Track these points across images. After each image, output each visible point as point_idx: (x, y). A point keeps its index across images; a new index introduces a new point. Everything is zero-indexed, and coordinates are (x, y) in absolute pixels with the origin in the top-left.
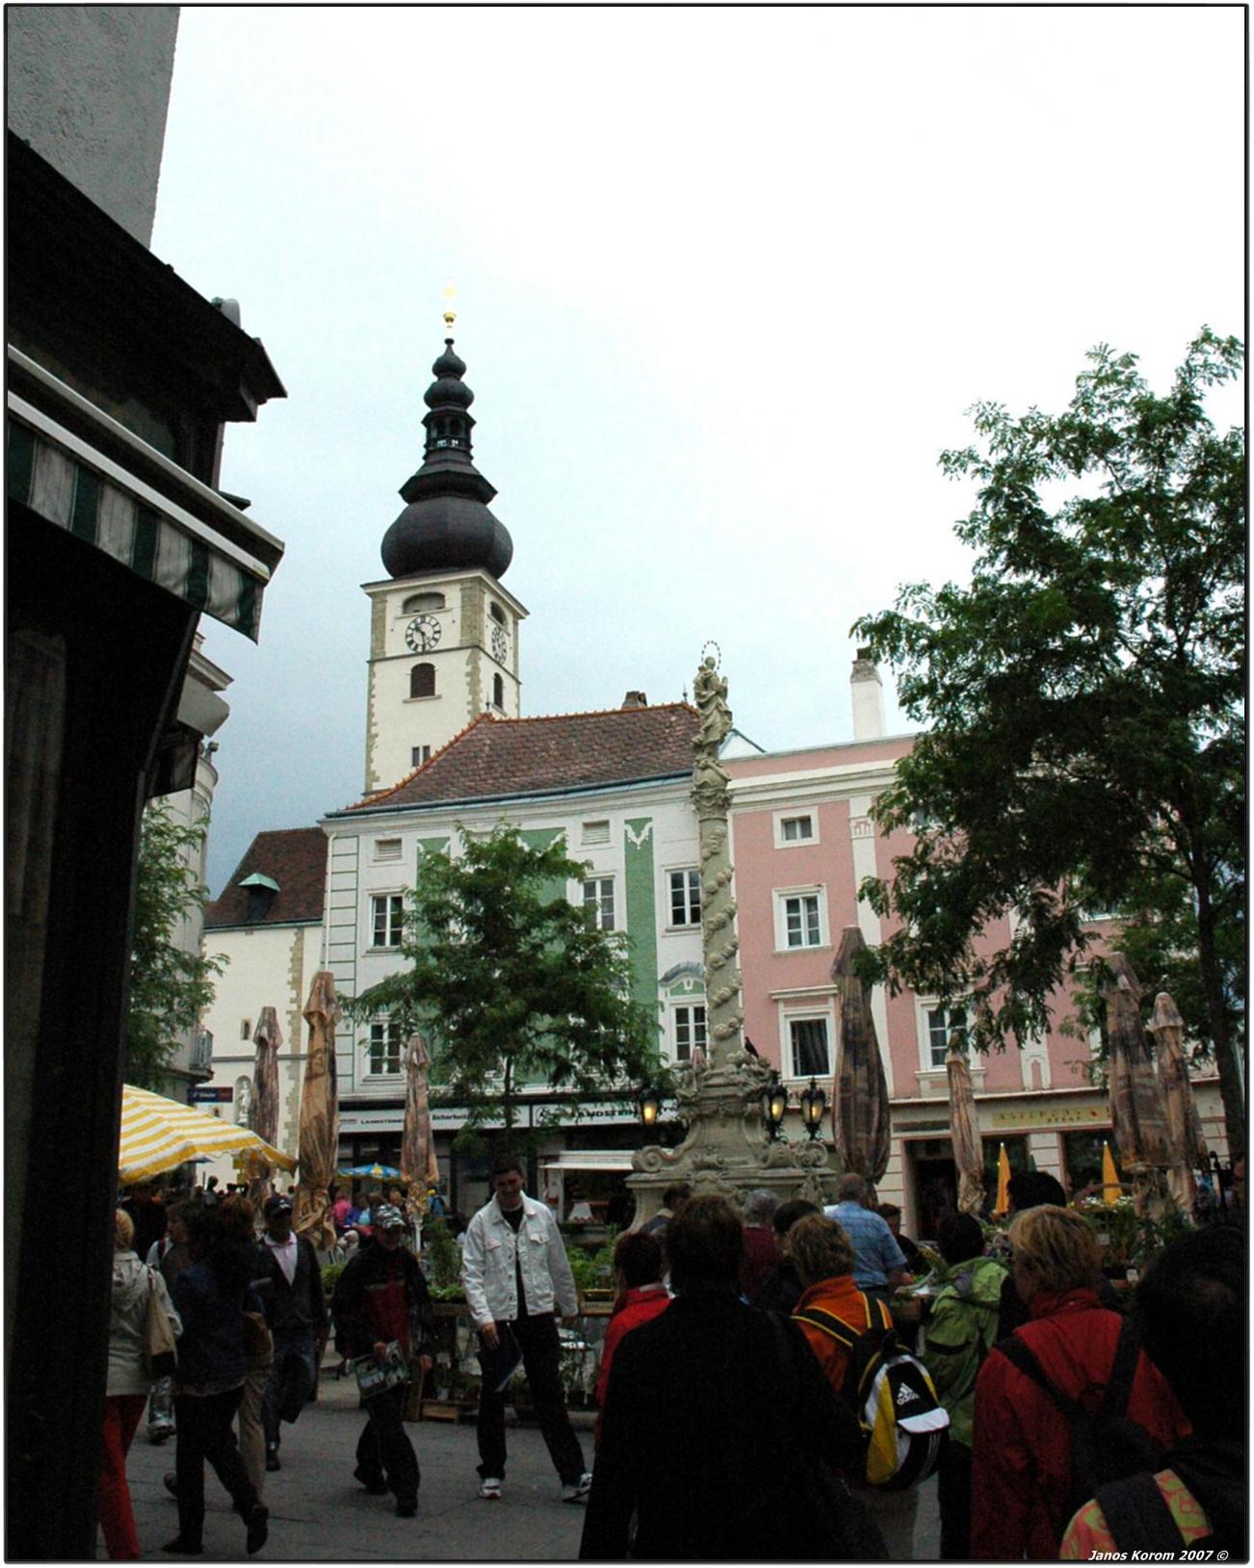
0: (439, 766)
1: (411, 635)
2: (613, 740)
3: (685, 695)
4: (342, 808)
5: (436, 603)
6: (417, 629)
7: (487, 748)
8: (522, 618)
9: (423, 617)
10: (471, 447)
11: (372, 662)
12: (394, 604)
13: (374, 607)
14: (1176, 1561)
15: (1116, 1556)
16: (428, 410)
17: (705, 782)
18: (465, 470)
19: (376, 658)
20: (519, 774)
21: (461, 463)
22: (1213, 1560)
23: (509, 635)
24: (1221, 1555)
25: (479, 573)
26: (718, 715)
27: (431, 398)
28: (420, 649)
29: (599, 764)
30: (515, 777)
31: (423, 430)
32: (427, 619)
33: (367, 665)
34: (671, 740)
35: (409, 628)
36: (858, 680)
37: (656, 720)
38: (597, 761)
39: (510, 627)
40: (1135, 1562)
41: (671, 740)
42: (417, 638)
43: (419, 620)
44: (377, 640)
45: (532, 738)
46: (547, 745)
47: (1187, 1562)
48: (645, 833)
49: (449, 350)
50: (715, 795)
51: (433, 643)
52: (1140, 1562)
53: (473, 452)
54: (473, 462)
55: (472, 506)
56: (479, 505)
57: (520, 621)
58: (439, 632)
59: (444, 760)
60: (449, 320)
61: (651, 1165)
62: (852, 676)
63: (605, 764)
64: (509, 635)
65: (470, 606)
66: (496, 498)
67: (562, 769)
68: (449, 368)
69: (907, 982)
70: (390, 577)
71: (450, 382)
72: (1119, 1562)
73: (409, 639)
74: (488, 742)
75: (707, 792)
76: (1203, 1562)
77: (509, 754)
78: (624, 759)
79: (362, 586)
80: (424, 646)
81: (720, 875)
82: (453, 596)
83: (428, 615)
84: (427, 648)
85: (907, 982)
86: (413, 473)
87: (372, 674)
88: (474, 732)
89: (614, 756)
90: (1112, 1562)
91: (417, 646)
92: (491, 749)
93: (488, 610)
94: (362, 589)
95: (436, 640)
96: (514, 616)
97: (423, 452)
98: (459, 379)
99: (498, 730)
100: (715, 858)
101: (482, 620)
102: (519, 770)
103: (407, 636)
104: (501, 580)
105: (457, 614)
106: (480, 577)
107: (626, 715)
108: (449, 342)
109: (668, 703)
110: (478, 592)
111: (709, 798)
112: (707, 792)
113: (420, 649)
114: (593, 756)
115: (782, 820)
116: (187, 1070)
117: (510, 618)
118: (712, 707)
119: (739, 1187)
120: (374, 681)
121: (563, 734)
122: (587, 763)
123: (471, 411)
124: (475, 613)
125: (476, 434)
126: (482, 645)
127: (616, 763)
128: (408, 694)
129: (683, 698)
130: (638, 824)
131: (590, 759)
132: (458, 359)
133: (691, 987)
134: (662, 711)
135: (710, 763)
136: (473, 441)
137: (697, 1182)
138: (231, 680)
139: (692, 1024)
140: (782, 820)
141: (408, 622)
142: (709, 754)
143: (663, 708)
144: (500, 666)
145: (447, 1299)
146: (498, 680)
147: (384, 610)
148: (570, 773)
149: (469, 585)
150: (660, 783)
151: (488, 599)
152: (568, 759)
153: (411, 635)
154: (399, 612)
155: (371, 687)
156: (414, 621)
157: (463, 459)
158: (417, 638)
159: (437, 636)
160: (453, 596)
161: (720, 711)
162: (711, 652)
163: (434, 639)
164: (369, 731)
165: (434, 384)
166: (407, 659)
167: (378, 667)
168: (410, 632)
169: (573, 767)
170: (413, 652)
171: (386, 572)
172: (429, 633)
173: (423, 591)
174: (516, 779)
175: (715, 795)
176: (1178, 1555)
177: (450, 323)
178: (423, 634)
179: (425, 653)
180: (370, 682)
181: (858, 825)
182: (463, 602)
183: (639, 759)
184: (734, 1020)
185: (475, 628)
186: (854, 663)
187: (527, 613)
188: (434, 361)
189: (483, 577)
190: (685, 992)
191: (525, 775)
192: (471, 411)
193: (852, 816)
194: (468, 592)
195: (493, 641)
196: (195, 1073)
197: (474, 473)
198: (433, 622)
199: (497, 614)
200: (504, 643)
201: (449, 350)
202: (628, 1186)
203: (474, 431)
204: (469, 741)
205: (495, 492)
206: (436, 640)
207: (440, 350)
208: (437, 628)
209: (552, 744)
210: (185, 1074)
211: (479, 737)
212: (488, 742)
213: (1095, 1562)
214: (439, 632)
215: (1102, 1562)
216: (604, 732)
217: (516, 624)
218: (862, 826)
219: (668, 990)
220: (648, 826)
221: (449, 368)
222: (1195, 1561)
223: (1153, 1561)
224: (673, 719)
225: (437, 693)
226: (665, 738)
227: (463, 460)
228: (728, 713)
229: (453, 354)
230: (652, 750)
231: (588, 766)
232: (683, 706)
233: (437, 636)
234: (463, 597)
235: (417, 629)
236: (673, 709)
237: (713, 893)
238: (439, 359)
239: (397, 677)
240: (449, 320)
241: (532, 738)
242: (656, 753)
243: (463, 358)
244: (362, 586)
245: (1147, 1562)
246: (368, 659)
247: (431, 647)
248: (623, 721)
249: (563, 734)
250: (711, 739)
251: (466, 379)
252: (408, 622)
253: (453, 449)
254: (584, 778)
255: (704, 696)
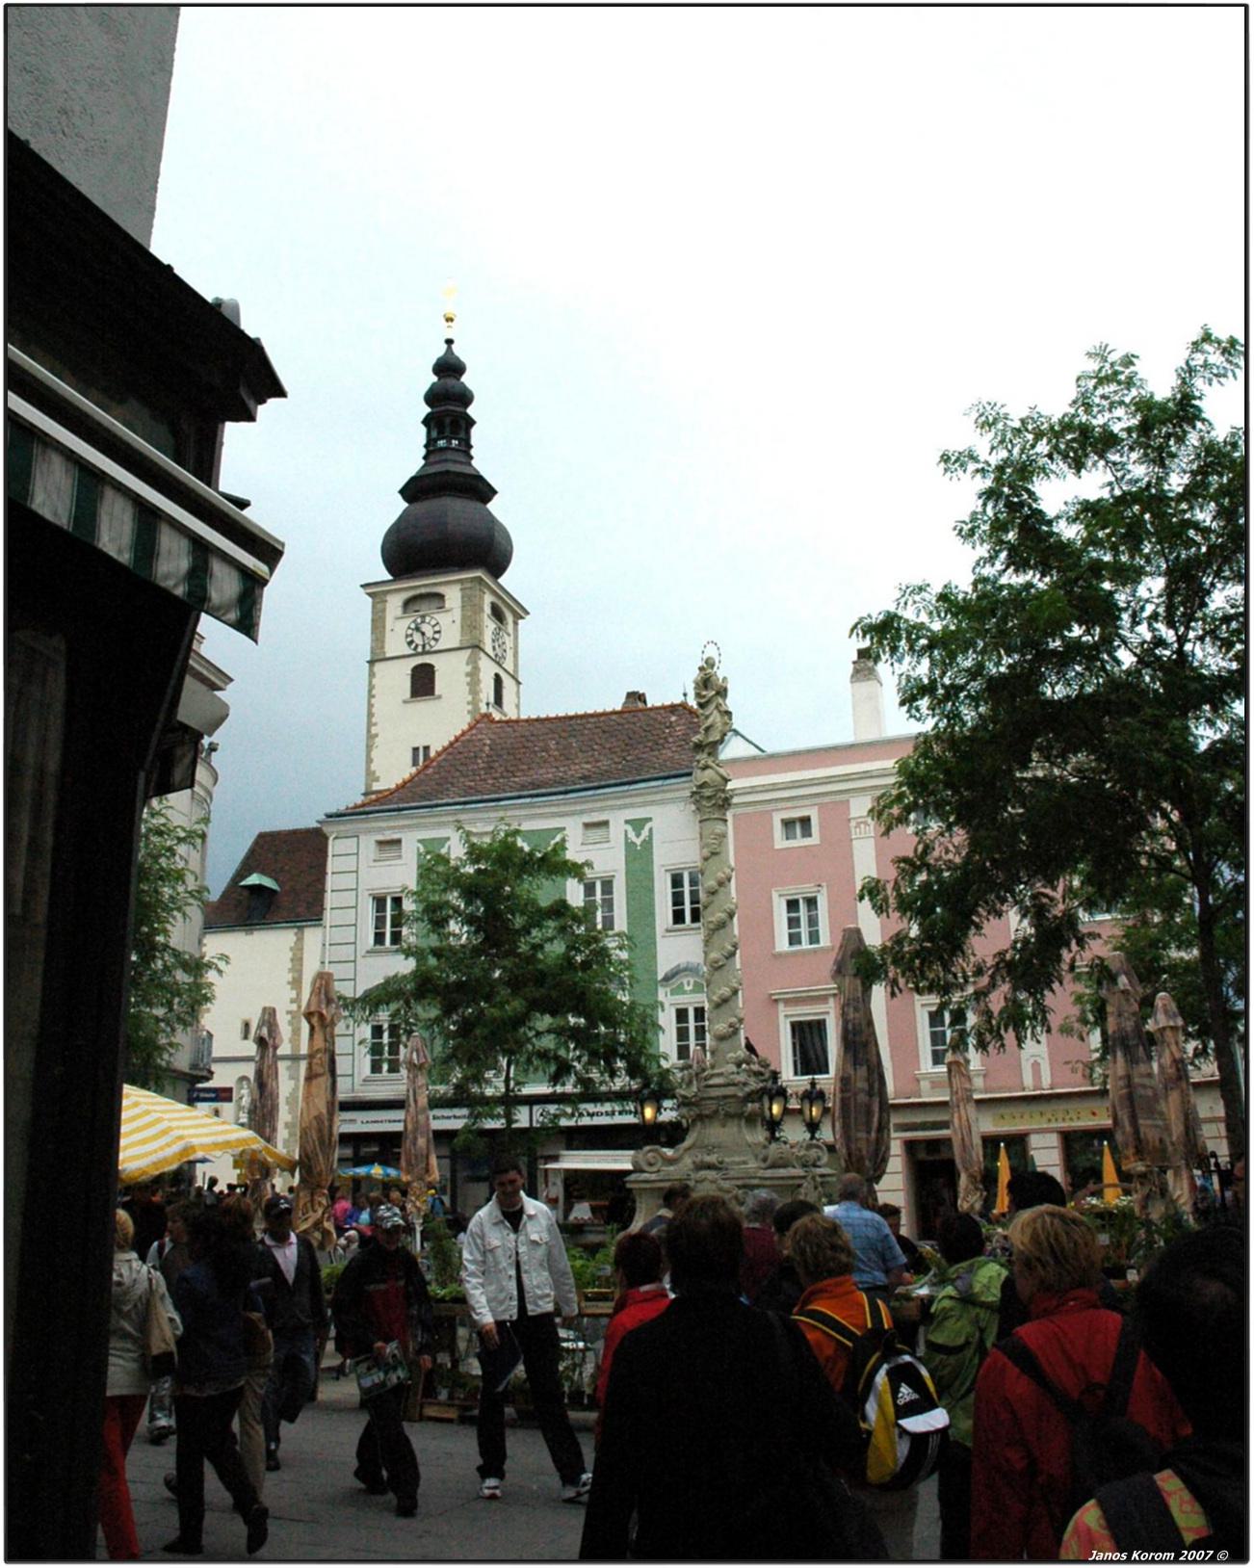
0: (439, 766)
1: (411, 635)
2: (613, 740)
3: (685, 695)
4: (342, 808)
5: (436, 603)
6: (417, 629)
7: (487, 748)
8: (522, 618)
9: (423, 617)
10: (471, 447)
11: (372, 662)
12: (394, 604)
13: (374, 607)
14: (1176, 1561)
15: (1116, 1556)
16: (428, 410)
17: (705, 782)
18: (465, 470)
19: (376, 658)
20: (519, 774)
21: (461, 463)
22: (1213, 1560)
23: (509, 635)
24: (1221, 1555)
25: (479, 573)
26: (718, 715)
27: (431, 398)
28: (420, 649)
29: (599, 764)
30: (515, 777)
31: (423, 430)
32: (427, 619)
33: (367, 665)
34: (671, 740)
35: (409, 628)
36: (858, 680)
37: (656, 720)
38: (597, 761)
39: (510, 627)
40: (1135, 1562)
41: (671, 740)
42: (417, 638)
43: (419, 620)
44: (377, 640)
45: (532, 738)
46: (547, 745)
47: (1187, 1562)
48: (645, 833)
49: (449, 350)
50: (715, 795)
51: (433, 643)
52: (1140, 1562)
53: (473, 452)
54: (473, 462)
55: (472, 506)
56: (479, 505)
57: (520, 621)
58: (439, 632)
59: (444, 760)
60: (449, 320)
61: (651, 1165)
62: (852, 676)
63: (605, 764)
64: (509, 635)
65: (470, 606)
66: (496, 498)
67: (562, 769)
68: (449, 368)
69: (907, 982)
70: (390, 577)
71: (450, 382)
72: (1119, 1562)
73: (409, 639)
74: (488, 742)
75: (707, 792)
76: (1203, 1562)
77: (509, 754)
78: (624, 759)
79: (362, 586)
80: (424, 646)
81: (720, 875)
82: (453, 596)
83: (428, 615)
84: (427, 648)
85: (907, 982)
86: (413, 473)
87: (372, 674)
88: (474, 732)
89: (614, 756)
90: (1112, 1562)
91: (417, 646)
92: (491, 749)
93: (488, 610)
94: (362, 589)
95: (436, 640)
96: (514, 616)
97: (423, 452)
98: (459, 379)
99: (498, 730)
100: (715, 858)
101: (482, 620)
102: (519, 770)
103: (407, 636)
104: (501, 580)
105: (457, 614)
106: (480, 577)
107: (626, 715)
108: (449, 342)
109: (668, 703)
110: (478, 592)
111: (709, 798)
112: (707, 792)
113: (420, 649)
114: (593, 756)
115: (782, 820)
116: (187, 1070)
117: (510, 618)
118: (712, 707)
119: (739, 1187)
120: (374, 681)
121: (563, 734)
122: (587, 763)
123: (471, 411)
124: (475, 613)
125: (476, 434)
126: (482, 645)
127: (616, 763)
128: (408, 694)
129: (683, 698)
130: (638, 824)
131: (590, 759)
132: (458, 359)
133: (691, 987)
134: (662, 711)
135: (710, 763)
136: (473, 441)
137: (697, 1182)
138: (231, 680)
139: (692, 1024)
140: (782, 820)
141: (408, 622)
142: (709, 754)
143: (663, 708)
144: (500, 666)
145: (447, 1299)
146: (498, 680)
147: (384, 610)
148: (570, 773)
149: (469, 585)
150: (660, 783)
151: (488, 599)
152: (568, 759)
153: (411, 635)
154: (399, 612)
155: (371, 687)
156: (414, 621)
157: (463, 459)
158: (417, 638)
159: (437, 636)
160: (453, 596)
161: (720, 711)
162: (711, 652)
163: (434, 639)
164: (369, 731)
165: (434, 384)
166: (407, 659)
167: (378, 667)
168: (410, 632)
169: (573, 767)
170: (413, 652)
171: (386, 572)
172: (429, 633)
173: (423, 591)
174: (516, 779)
175: (715, 795)
176: (1178, 1555)
177: (450, 323)
178: (423, 634)
179: (425, 653)
180: (370, 682)
181: (858, 825)
182: (463, 602)
183: (639, 759)
184: (734, 1020)
185: (475, 628)
186: (854, 663)
187: (527, 613)
188: (434, 361)
189: (483, 577)
190: (685, 992)
191: (525, 775)
192: (471, 411)
193: (852, 816)
194: (468, 592)
195: (493, 641)
196: (195, 1073)
197: (474, 473)
198: (433, 622)
199: (497, 614)
200: (504, 643)
201: (449, 350)
202: (628, 1186)
203: (474, 431)
204: (469, 741)
205: (495, 492)
206: (436, 640)
207: (440, 350)
208: (437, 628)
209: (552, 744)
210: (185, 1074)
211: (479, 737)
212: (488, 742)
213: (1095, 1562)
214: (439, 632)
215: (1102, 1562)
216: (604, 732)
217: (516, 624)
218: (862, 826)
219: (668, 990)
220: (648, 826)
221: (449, 368)
222: (1195, 1561)
223: (1153, 1561)
224: (673, 719)
225: (437, 693)
226: (665, 738)
227: (463, 460)
228: (728, 713)
229: (453, 354)
230: (652, 750)
231: (588, 766)
232: (683, 706)
233: (437, 636)
234: (463, 597)
235: (417, 629)
236: (673, 709)
237: (713, 893)
238: (439, 359)
239: (397, 677)
240: (449, 320)
241: (532, 738)
242: (656, 753)
243: (463, 358)
244: (362, 586)
245: (1147, 1562)
246: (368, 659)
247: (431, 647)
248: (623, 721)
249: (563, 734)
250: (711, 739)
251: (466, 379)
252: (408, 622)
253: (453, 449)
254: (584, 778)
255: (704, 696)
